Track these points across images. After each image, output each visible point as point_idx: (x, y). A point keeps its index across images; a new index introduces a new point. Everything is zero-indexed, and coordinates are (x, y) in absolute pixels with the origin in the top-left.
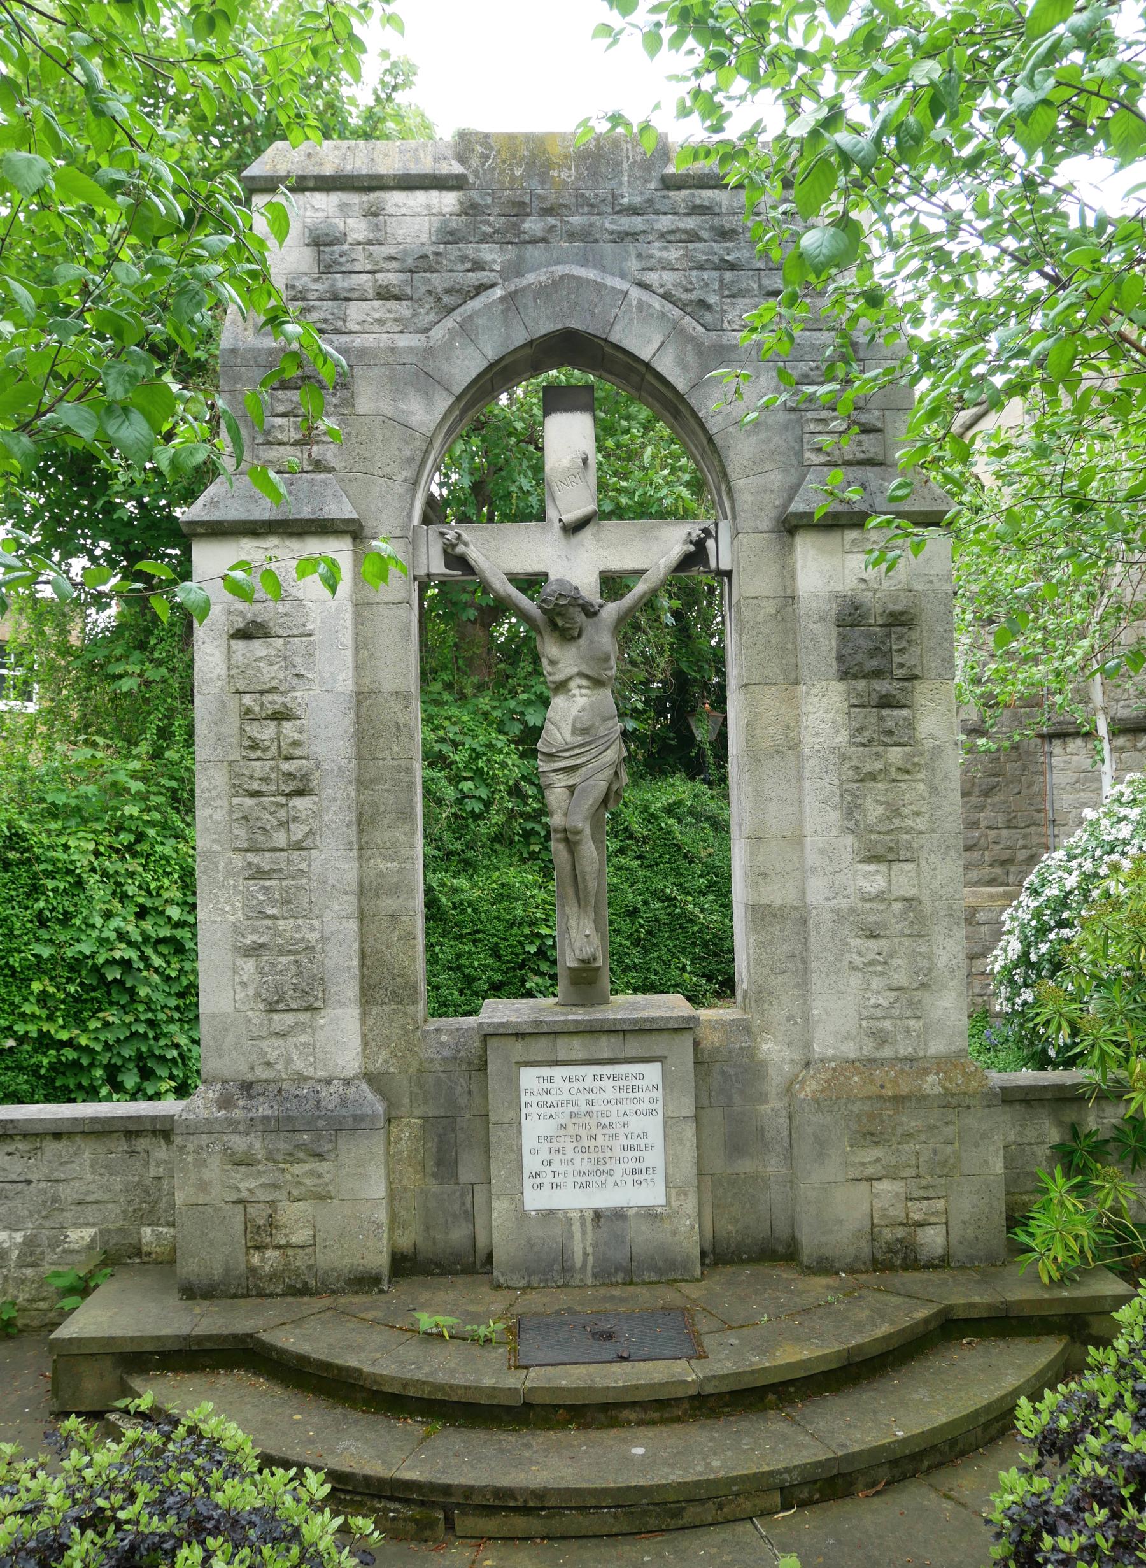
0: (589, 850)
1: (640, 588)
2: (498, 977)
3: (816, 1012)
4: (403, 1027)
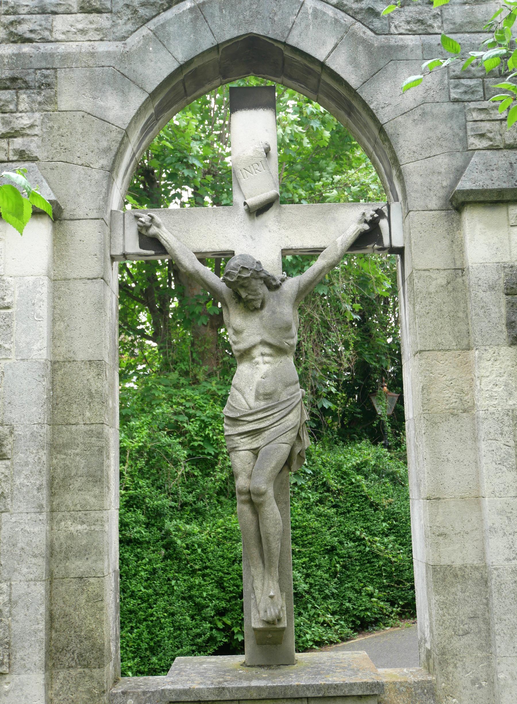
0: (272, 511)
1: (319, 264)
2: (223, 604)
3: (501, 676)
4: (89, 691)
